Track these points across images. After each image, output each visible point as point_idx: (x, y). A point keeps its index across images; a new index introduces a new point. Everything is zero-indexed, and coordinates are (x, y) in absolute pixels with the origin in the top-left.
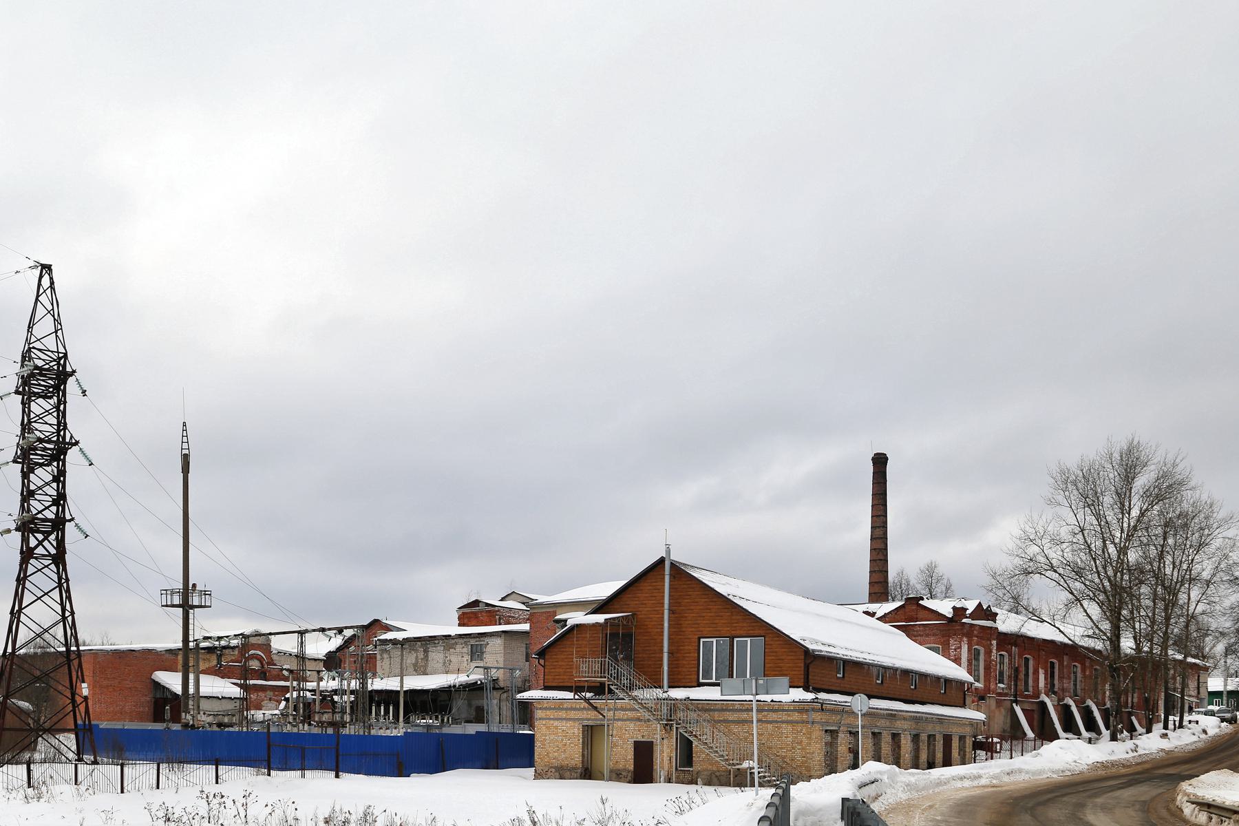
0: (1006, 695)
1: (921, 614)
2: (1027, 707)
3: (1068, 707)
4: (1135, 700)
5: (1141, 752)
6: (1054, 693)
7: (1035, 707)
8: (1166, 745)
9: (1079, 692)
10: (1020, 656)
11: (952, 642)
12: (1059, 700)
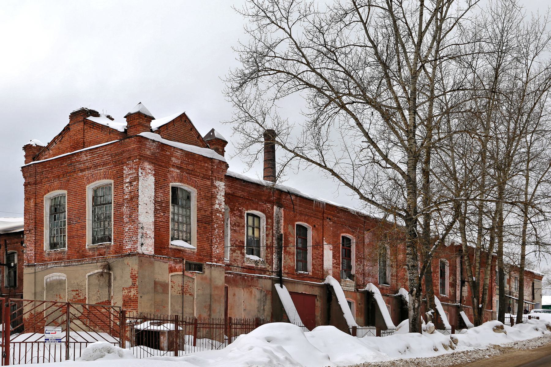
0: (263, 271)
1: (91, 134)
2: (300, 289)
3: (369, 295)
4: (465, 294)
5: (460, 348)
6: (351, 277)
7: (316, 292)
8: (500, 340)
9: (389, 279)
10: (289, 221)
11: (126, 171)
12: (358, 286)
